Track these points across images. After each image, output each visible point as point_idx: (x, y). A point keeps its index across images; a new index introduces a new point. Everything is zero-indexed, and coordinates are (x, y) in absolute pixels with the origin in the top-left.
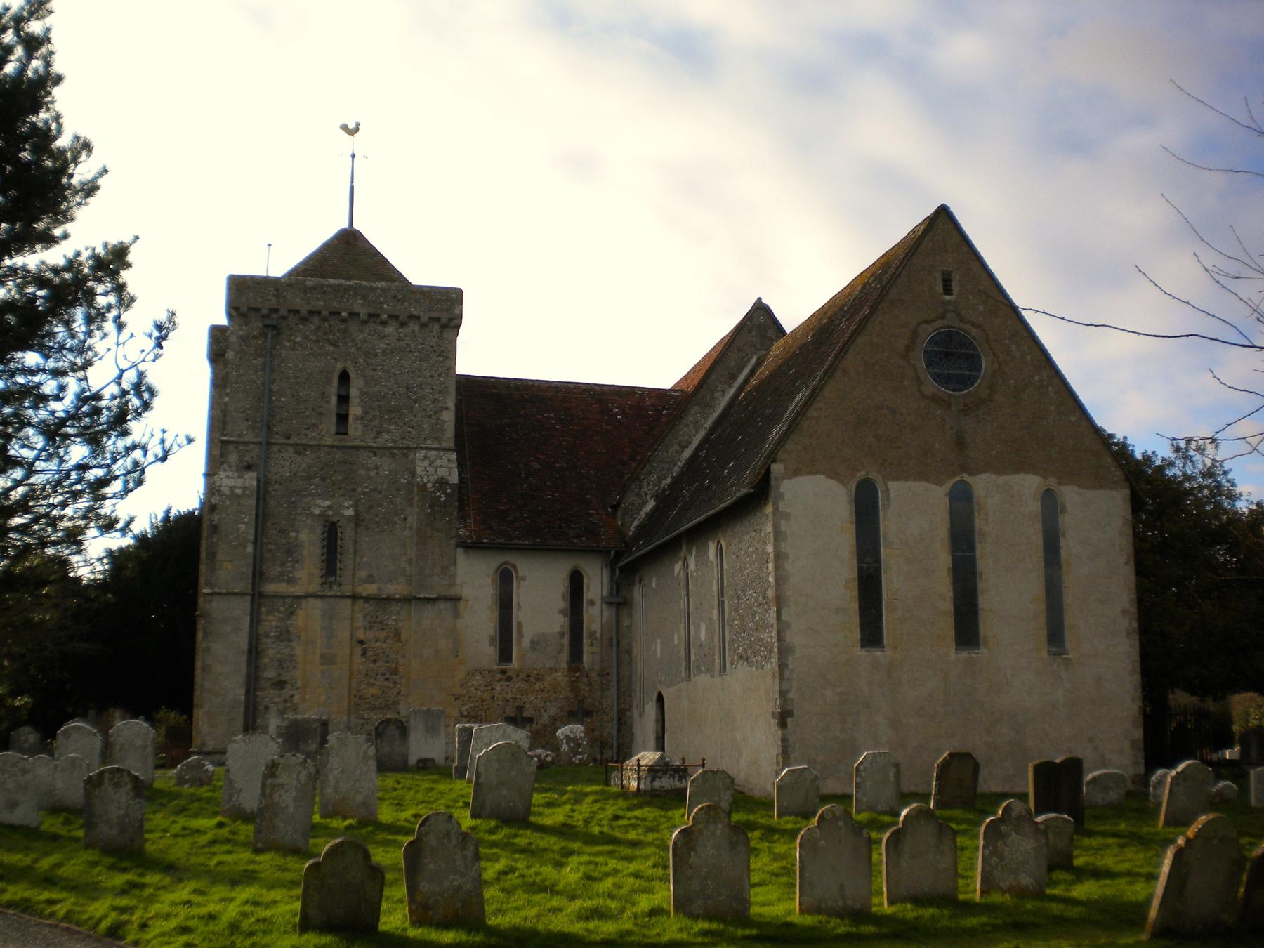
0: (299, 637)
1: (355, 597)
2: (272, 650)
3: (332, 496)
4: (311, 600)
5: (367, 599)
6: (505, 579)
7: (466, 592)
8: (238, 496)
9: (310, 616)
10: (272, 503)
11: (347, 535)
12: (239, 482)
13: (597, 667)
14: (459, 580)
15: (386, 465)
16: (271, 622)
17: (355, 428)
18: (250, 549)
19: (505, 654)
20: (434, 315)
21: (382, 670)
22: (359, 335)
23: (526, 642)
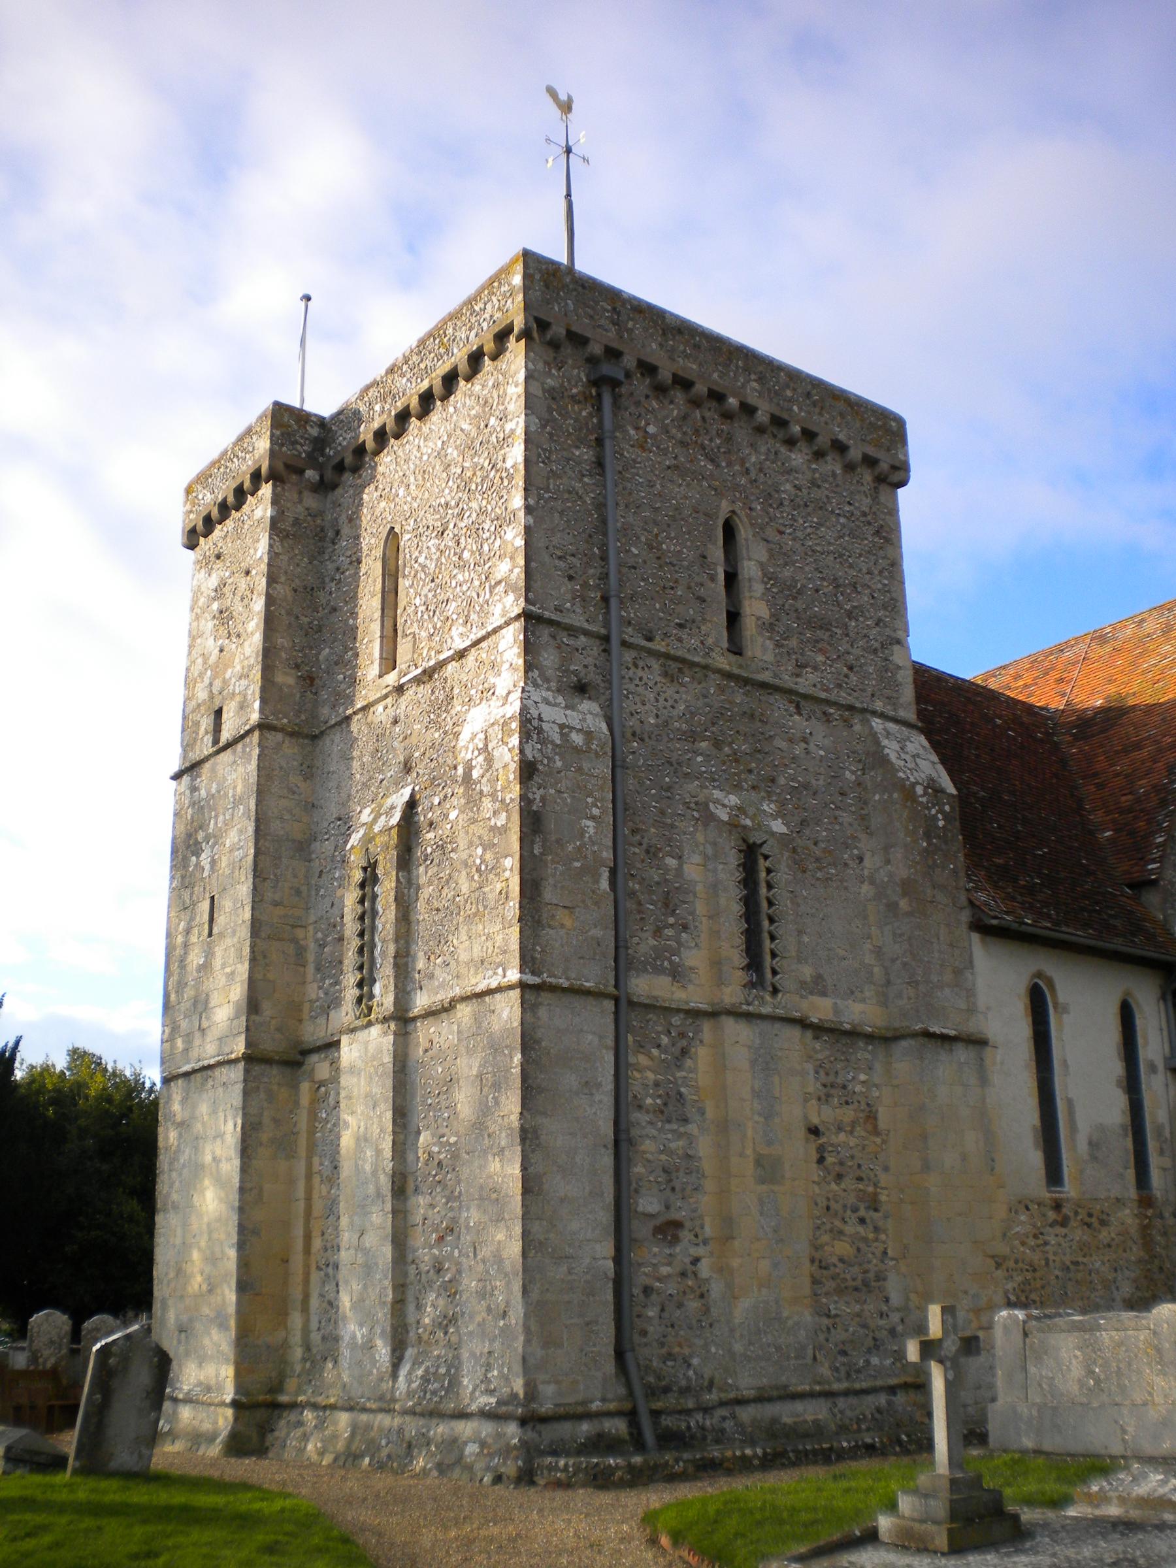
0: (702, 1112)
2: (651, 1143)
4: (729, 1023)
5: (818, 1030)
6: (1038, 1005)
8: (577, 750)
14: (982, 1000)
15: (821, 737)
16: (645, 1071)
17: (760, 648)
18: (604, 884)
19: (1054, 1175)
20: (871, 451)
21: (852, 1200)
23: (1083, 1146)
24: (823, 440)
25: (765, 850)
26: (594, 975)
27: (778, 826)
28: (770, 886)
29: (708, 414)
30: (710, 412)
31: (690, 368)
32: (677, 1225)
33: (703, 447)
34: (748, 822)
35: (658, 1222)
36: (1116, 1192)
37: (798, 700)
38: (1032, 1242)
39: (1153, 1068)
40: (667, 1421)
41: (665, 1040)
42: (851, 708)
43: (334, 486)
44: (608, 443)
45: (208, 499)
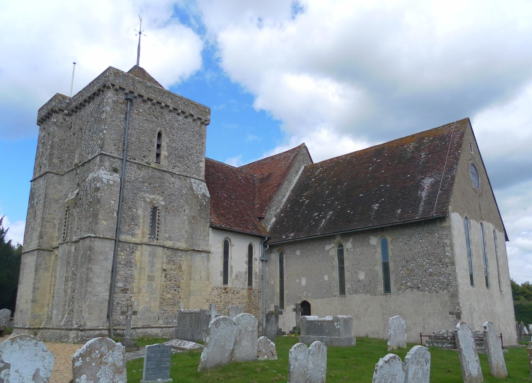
1: (164, 247)
2: (122, 272)
3: (154, 194)
4: (144, 246)
5: (168, 248)
7: (212, 249)
9: (142, 255)
10: (126, 192)
11: (162, 214)
12: (111, 178)
13: (257, 288)
14: (210, 243)
15: (178, 183)
16: (122, 256)
17: (164, 163)
18: (115, 215)
19: (226, 281)
20: (199, 116)
21: (173, 285)
22: (169, 117)
24: (187, 114)
25: (158, 208)
26: (111, 234)
27: (163, 203)
28: (159, 216)
29: (157, 107)
30: (158, 107)
31: (152, 96)
32: (128, 289)
33: (154, 115)
34: (155, 202)
35: (122, 289)
36: (242, 286)
37: (172, 174)
38: (217, 296)
39: (256, 260)
40: (118, 331)
41: (128, 249)
42: (187, 176)
43: (71, 115)
44: (128, 114)
45: (43, 113)
